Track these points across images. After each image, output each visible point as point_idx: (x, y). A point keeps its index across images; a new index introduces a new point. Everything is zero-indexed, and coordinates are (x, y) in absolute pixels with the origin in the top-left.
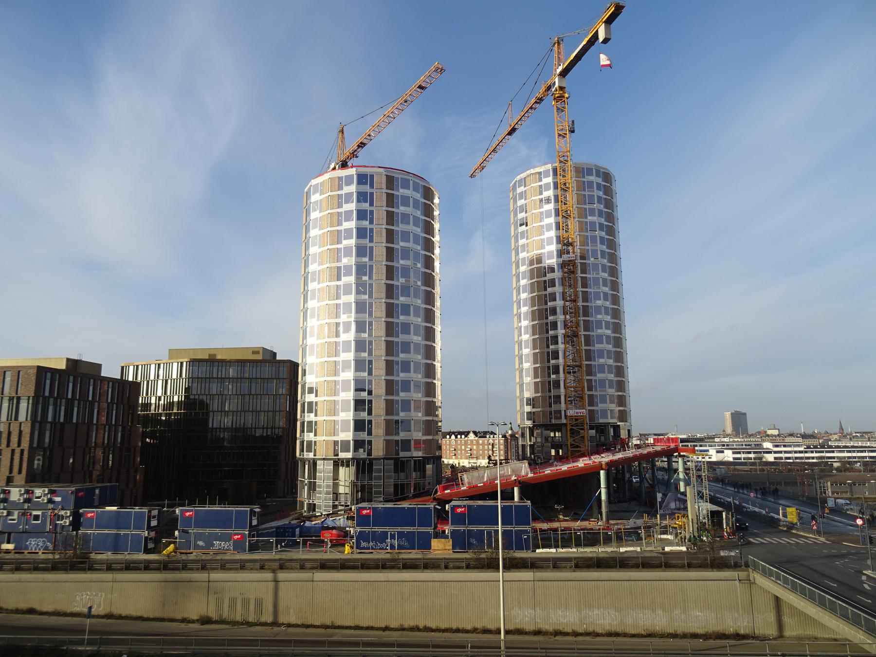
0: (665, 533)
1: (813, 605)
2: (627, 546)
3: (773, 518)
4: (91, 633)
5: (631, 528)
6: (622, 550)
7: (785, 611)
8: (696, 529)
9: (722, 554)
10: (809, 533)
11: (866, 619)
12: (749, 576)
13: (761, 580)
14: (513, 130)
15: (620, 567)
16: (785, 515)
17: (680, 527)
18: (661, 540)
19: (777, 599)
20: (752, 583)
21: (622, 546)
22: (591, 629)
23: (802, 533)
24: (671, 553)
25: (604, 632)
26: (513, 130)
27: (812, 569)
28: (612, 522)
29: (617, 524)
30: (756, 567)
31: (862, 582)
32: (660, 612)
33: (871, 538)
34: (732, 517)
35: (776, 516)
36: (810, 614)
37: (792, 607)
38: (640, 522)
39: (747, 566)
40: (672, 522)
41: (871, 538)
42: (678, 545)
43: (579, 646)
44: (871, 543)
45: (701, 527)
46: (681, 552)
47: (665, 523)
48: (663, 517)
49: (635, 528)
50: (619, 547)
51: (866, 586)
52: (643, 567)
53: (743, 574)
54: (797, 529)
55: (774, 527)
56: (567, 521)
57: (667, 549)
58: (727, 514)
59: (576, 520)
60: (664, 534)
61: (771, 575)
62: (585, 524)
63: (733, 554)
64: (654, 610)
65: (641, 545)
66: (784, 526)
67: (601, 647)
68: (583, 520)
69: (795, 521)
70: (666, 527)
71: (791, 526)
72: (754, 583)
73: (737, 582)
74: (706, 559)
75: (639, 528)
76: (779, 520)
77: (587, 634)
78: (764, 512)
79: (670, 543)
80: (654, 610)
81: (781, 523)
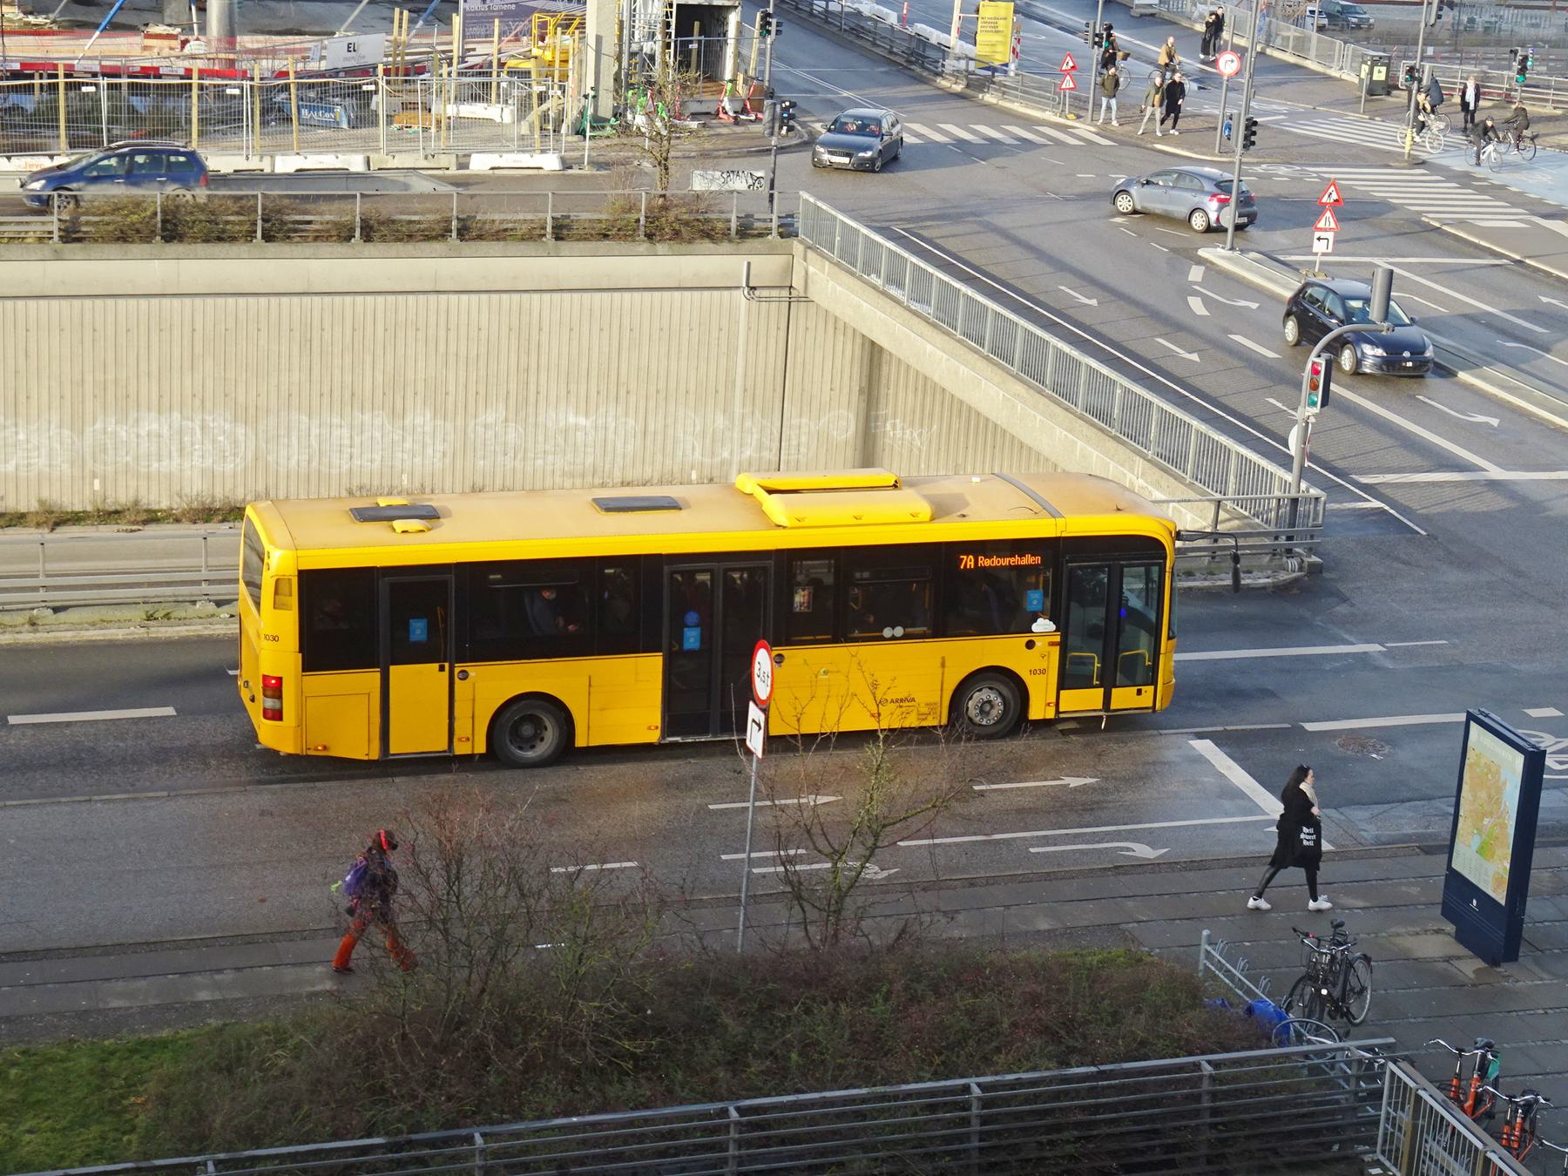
0: (480, 94)
1: (999, 375)
2: (306, 147)
3: (923, 42)
4: (1547, 100)
5: (335, 73)
6: (286, 164)
7: (888, 371)
8: (608, 82)
9: (699, 183)
10: (1041, 103)
11: (1167, 422)
12: (789, 269)
13: (831, 287)
14: (943, 665)
15: (268, 237)
16: (969, 36)
17: (547, 71)
18: (460, 123)
19: (874, 354)
20: (792, 296)
21: (286, 149)
22: (121, 496)
23: (1017, 107)
24: (494, 179)
25: (178, 505)
26: (943, 665)
27: (1017, 242)
28: (247, 41)
29: (272, 52)
30: (821, 241)
31: (1188, 290)
32: (421, 419)
33: (1251, 125)
34: (765, 31)
35: (935, 36)
36: (985, 408)
37: (926, 386)
38: (374, 47)
39: (787, 231)
40: (516, 49)
41: (1251, 125)
42: (525, 145)
43: (53, 567)
44: (1249, 143)
45: (633, 75)
46: (534, 178)
47: (485, 50)
48: (478, 24)
49: (349, 72)
50: (270, 152)
51: (1196, 304)
52: (367, 237)
53: (765, 265)
54: (1004, 90)
55: (921, 80)
56: (37, 31)
57: (480, 163)
58: (746, 19)
59: (80, 27)
60: (475, 98)
61: (870, 267)
62: (128, 49)
63: (740, 184)
64: (396, 414)
65: (368, 146)
66: (956, 74)
67: (165, 563)
68: (116, 27)
69: (1002, 55)
70: (483, 70)
71: (984, 77)
72: (806, 299)
73: (740, 297)
74: (632, 207)
75: (367, 71)
76: (942, 50)
77: (110, 516)
78: (892, 18)
79: (494, 138)
80: (396, 414)
81: (950, 64)
